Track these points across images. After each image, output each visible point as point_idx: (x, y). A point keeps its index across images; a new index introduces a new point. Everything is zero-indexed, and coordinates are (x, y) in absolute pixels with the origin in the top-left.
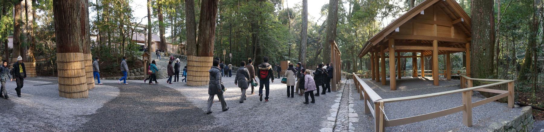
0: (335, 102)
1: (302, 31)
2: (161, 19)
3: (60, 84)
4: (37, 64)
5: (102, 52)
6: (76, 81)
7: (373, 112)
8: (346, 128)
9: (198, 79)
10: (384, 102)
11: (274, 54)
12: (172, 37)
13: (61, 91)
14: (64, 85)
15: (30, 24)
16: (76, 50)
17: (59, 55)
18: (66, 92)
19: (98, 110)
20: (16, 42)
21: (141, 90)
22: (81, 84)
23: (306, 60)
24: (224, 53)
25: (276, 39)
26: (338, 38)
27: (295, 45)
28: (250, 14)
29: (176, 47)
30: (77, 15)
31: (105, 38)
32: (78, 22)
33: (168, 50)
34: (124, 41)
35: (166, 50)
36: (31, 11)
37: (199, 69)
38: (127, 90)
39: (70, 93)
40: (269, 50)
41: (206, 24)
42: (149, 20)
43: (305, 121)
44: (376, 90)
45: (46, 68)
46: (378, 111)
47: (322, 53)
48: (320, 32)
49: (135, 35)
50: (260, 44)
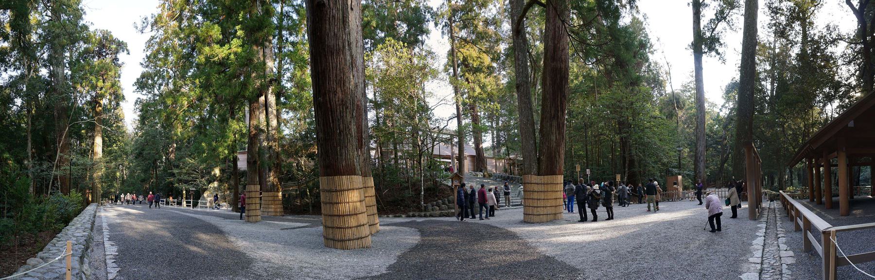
0: (758, 236)
1: (697, 128)
2: (475, 119)
3: (326, 227)
4: (283, 196)
5: (385, 175)
6: (352, 222)
7: (819, 249)
8: (778, 273)
9: (541, 211)
10: (837, 231)
11: (656, 166)
12: (493, 148)
13: (326, 238)
14: (332, 228)
15: (273, 132)
16: (352, 172)
17: (323, 182)
18: (335, 240)
19: (390, 267)
20: (252, 161)
21: (453, 232)
22: (360, 226)
23: (705, 173)
24: (578, 169)
25: (658, 143)
26: (754, 137)
27: (687, 150)
28: (616, 107)
29: (501, 164)
30: (352, 117)
31: (389, 153)
32: (353, 128)
33: (489, 168)
34: (420, 156)
35: (486, 168)
36: (275, 112)
37: (542, 196)
38: (431, 234)
39: (342, 241)
40: (648, 160)
41: (551, 125)
42: (459, 122)
43: (715, 266)
44: (819, 214)
45: (298, 202)
46: (827, 245)
47: (730, 160)
48: (725, 127)
49: (436, 147)
50: (634, 152)
